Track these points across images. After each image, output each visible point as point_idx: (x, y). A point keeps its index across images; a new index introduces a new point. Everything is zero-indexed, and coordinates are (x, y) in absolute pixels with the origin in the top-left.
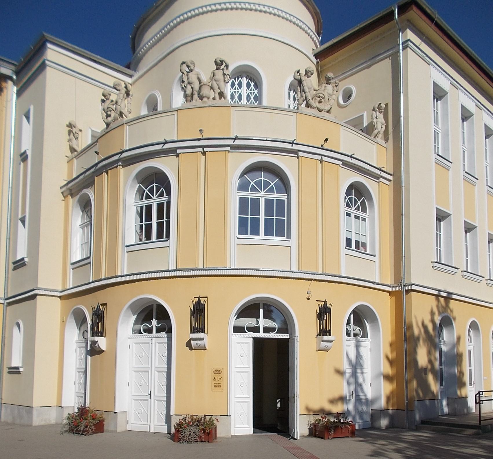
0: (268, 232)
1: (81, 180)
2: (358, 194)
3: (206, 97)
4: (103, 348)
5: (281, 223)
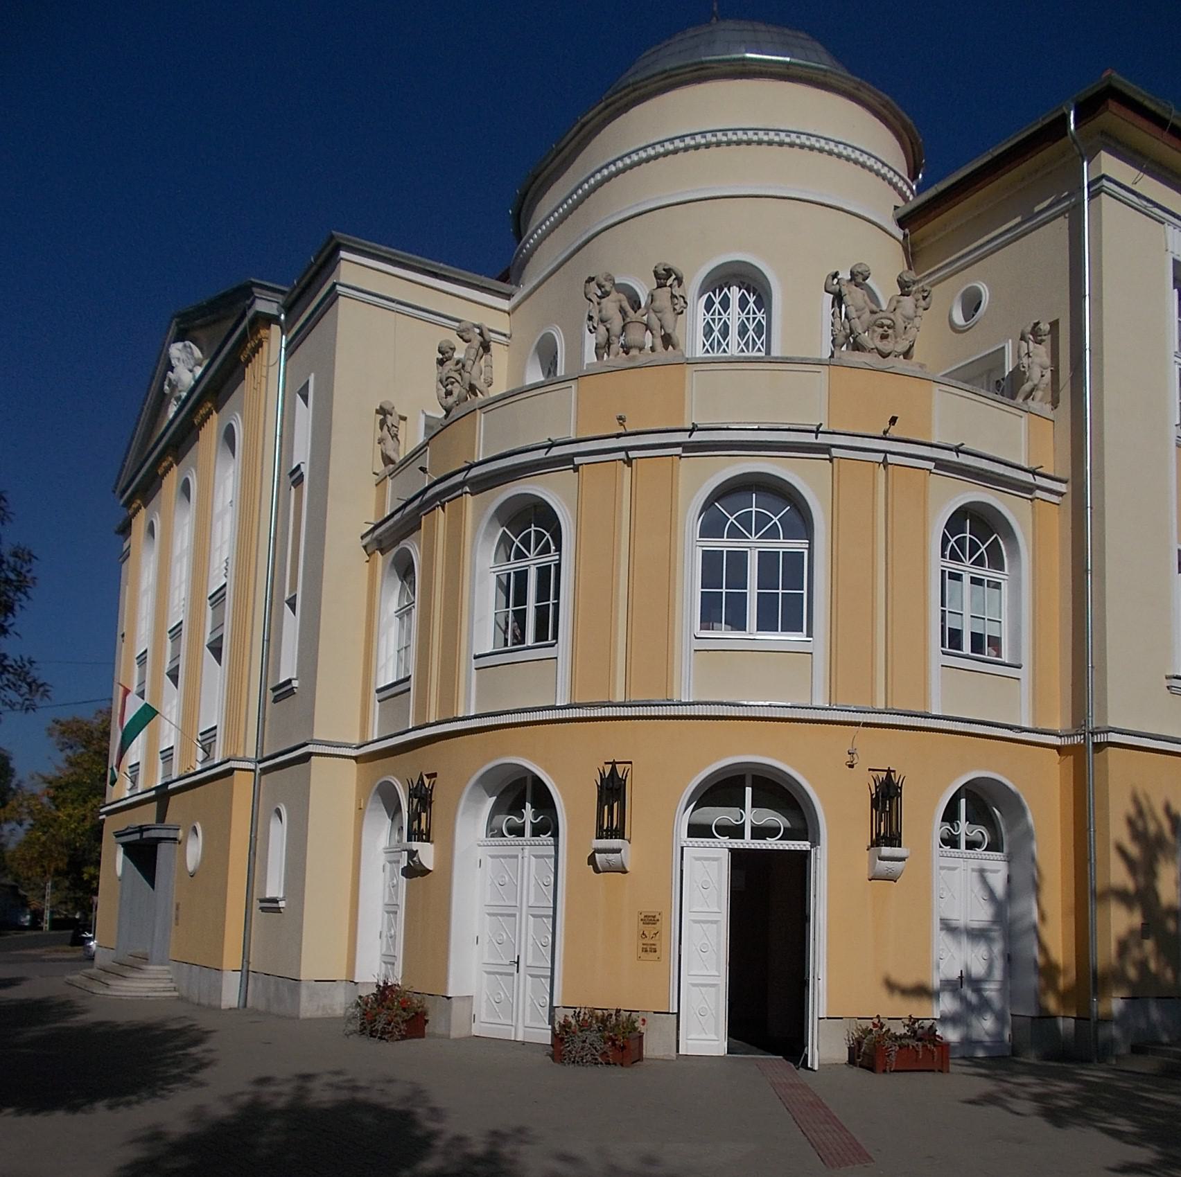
0: (766, 623)
1: (396, 523)
2: (977, 533)
3: (635, 347)
4: (429, 863)
5: (794, 603)
